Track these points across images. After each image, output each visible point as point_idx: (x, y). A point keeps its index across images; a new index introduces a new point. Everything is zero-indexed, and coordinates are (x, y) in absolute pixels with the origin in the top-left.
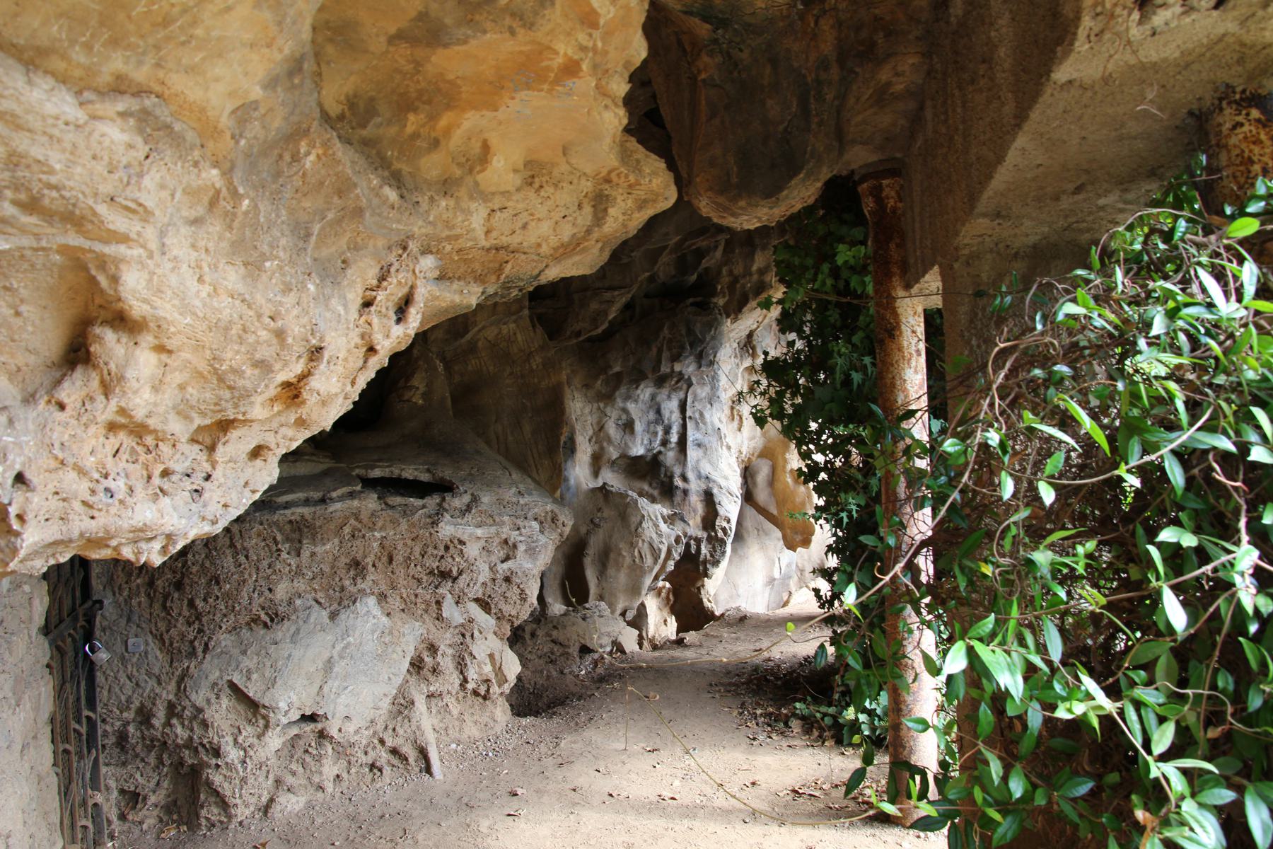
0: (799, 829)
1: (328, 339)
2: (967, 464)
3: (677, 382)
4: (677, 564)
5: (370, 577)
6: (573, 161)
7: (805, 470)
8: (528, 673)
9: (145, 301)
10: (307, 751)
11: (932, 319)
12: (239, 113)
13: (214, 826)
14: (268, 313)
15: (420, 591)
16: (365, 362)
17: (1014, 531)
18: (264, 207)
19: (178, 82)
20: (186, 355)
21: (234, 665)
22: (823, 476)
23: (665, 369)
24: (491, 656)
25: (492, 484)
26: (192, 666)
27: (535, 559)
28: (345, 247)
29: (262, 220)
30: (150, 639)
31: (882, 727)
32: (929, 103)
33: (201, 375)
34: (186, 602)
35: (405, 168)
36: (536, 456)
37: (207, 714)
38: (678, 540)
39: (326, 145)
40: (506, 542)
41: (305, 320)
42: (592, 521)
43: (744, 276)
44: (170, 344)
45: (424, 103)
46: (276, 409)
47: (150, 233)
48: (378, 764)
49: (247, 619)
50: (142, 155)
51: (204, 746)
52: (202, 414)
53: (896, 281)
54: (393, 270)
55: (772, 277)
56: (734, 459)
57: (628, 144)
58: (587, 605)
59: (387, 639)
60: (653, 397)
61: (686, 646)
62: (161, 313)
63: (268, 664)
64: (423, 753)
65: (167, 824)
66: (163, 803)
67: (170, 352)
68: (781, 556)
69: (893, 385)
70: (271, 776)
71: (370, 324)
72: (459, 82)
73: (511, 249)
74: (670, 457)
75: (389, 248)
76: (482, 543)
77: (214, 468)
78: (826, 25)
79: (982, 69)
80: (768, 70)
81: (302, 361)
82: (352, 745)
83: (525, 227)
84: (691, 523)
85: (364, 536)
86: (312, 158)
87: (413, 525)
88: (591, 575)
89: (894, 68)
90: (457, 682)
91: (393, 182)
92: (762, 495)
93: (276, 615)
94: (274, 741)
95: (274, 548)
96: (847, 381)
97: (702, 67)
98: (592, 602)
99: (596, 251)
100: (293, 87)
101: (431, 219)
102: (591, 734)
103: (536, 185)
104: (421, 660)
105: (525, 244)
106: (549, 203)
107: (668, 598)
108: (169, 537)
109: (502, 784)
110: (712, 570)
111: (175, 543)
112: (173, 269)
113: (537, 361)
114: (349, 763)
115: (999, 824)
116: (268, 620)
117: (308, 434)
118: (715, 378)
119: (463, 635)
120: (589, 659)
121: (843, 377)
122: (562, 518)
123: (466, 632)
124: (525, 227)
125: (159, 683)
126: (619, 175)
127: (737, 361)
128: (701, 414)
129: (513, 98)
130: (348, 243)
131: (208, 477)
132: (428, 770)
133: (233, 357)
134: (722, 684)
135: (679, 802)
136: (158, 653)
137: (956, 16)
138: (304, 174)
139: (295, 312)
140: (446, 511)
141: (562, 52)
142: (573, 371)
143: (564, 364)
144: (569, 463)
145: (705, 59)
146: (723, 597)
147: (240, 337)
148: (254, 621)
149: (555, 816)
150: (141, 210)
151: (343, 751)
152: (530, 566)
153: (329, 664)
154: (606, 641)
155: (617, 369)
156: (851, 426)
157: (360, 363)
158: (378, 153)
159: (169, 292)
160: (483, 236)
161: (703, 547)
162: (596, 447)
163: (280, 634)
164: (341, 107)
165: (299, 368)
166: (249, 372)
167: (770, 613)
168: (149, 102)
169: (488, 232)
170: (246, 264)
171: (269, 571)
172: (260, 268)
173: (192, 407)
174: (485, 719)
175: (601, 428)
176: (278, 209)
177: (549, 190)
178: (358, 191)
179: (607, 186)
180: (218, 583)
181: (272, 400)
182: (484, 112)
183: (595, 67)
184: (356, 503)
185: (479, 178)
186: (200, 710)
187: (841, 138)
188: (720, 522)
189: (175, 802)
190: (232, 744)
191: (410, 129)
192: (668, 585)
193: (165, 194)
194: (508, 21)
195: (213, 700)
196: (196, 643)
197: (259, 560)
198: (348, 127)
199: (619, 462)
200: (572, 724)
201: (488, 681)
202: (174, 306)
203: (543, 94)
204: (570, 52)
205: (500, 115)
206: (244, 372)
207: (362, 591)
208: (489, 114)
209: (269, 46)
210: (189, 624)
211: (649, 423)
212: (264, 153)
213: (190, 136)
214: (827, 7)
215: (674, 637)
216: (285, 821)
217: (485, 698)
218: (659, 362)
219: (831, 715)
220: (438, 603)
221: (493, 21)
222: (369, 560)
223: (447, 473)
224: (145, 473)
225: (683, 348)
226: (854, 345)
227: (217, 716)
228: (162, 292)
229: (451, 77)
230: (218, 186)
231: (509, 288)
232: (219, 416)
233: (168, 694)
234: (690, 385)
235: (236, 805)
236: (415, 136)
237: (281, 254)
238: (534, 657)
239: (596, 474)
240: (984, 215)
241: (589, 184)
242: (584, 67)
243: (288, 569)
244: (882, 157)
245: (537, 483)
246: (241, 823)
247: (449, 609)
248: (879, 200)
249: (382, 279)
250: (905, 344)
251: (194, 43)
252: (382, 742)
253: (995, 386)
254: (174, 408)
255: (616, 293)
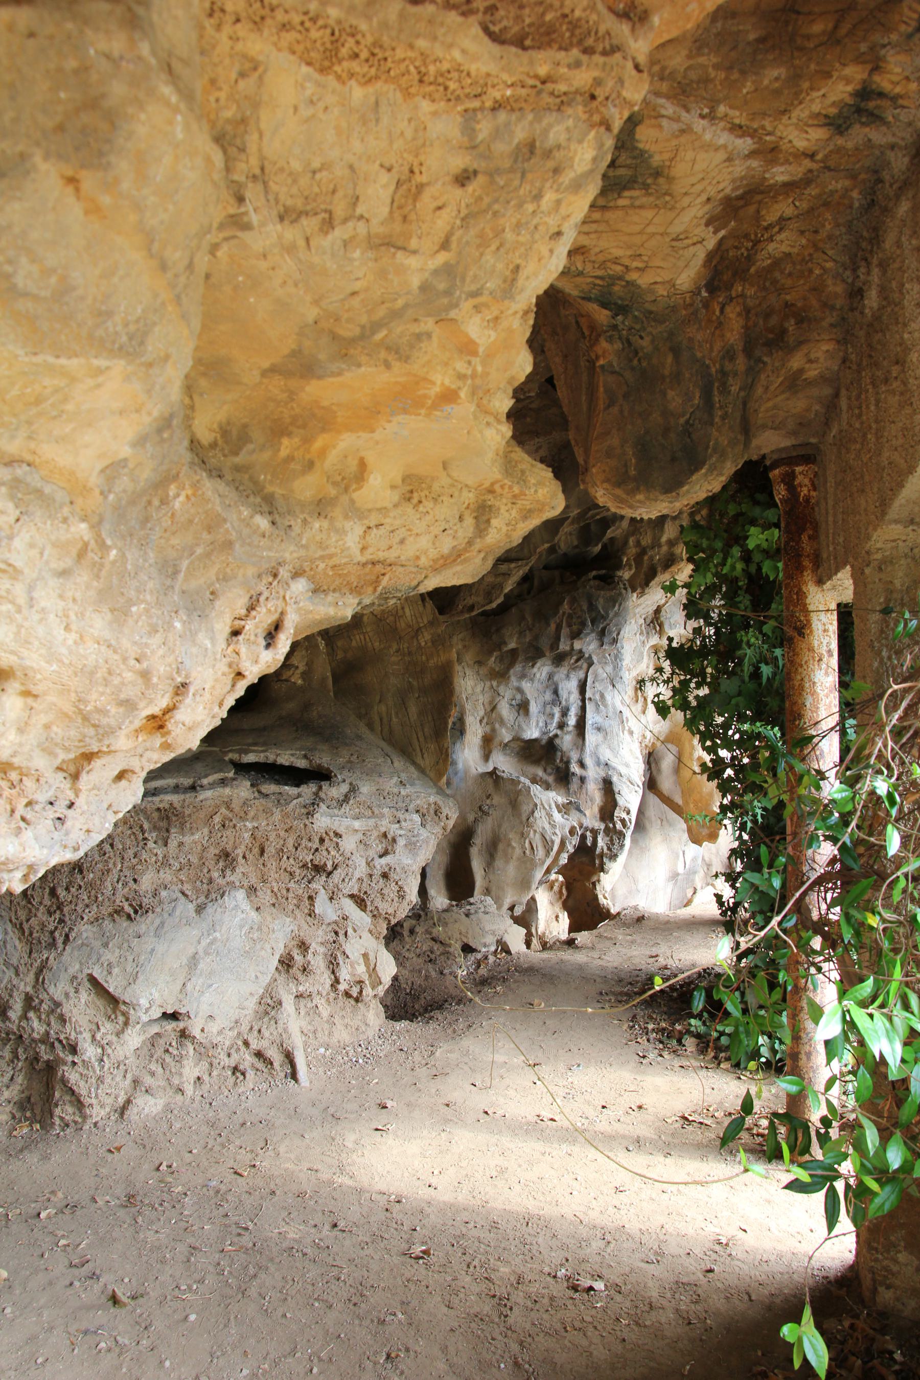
0: (686, 1162)
1: (194, 674)
2: (855, 810)
3: (577, 661)
4: (571, 858)
5: (239, 870)
6: (455, 474)
7: (710, 765)
8: (405, 972)
9: (13, 652)
10: (167, 1051)
11: (845, 614)
12: (108, 472)
13: (67, 1125)
14: (133, 655)
15: (292, 885)
16: (233, 686)
17: (902, 883)
18: (132, 555)
19: (48, 451)
20: (51, 698)
21: (94, 958)
22: (729, 772)
23: (564, 646)
24: (365, 956)
25: (373, 773)
26: (52, 958)
27: (415, 855)
28: (214, 578)
29: (129, 567)
30: (9, 927)
31: (783, 1052)
32: (843, 392)
33: (66, 715)
34: (47, 890)
35: (278, 491)
36: (422, 739)
37: (66, 1009)
38: (572, 831)
39: (195, 486)
40: (385, 835)
41: (171, 659)
42: (480, 808)
43: (653, 548)
44: (35, 690)
45: (298, 427)
46: (140, 739)
47: (19, 590)
48: (241, 1067)
49: (110, 910)
50: (12, 519)
51: (60, 1042)
52: (67, 749)
53: (808, 576)
54: (262, 599)
55: (681, 550)
56: (637, 745)
57: (513, 455)
58: (472, 900)
59: (256, 935)
60: (550, 677)
61: (577, 947)
62: (28, 663)
63: (130, 958)
64: (289, 1058)
65: (20, 1121)
66: (16, 1099)
67: (36, 696)
68: (686, 849)
69: (802, 688)
70: (129, 1076)
71: (237, 653)
72: (334, 408)
73: (388, 561)
74: (567, 741)
75: (259, 576)
76: (360, 836)
77: (77, 796)
78: (732, 312)
79: (895, 370)
80: (670, 359)
81: (168, 695)
82: (214, 1046)
83: (402, 542)
84: (587, 813)
85: (235, 826)
86: (182, 498)
87: (287, 815)
88: (477, 866)
89: (807, 355)
90: (328, 982)
91: (266, 508)
92: (666, 783)
93: (141, 906)
94: (134, 1039)
95: (141, 837)
96: (756, 674)
97: (600, 352)
98: (477, 896)
99: (478, 560)
100: (163, 441)
101: (304, 542)
102: (468, 1042)
103: (415, 501)
104: (291, 958)
105: (402, 558)
106: (428, 518)
107: (560, 892)
108: (31, 868)
109: (372, 1094)
110: (609, 865)
111: (36, 872)
112: (41, 620)
113: (426, 637)
114: (211, 1065)
115: (874, 1194)
116: (132, 912)
117: (172, 755)
118: (618, 657)
119: (336, 933)
120: (472, 957)
121: (752, 669)
122: (445, 811)
123: (339, 931)
124: (402, 542)
125: (17, 974)
126: (502, 487)
127: (643, 638)
128: (602, 696)
129: (390, 421)
130: (217, 574)
131: (71, 805)
132: (294, 1076)
133: (97, 698)
134: (614, 993)
135: (559, 1123)
136: (17, 942)
137: (871, 308)
138: (173, 514)
139: (161, 652)
140: (323, 800)
141: (439, 382)
142: (465, 647)
143: (455, 639)
144: (458, 745)
145: (604, 344)
146: (621, 892)
147: (105, 679)
148: (117, 912)
149: (425, 1132)
150: (10, 569)
151: (205, 1051)
152: (409, 862)
153: (194, 960)
154: (491, 940)
155: (512, 645)
156: (758, 724)
157: (229, 687)
158: (251, 478)
159: (36, 643)
160: (358, 553)
161: (600, 839)
162: (488, 729)
163: (143, 928)
164: (214, 435)
165: (164, 702)
166: (113, 710)
167: (670, 913)
168: (21, 471)
169: (363, 549)
170: (112, 611)
171: (135, 861)
172: (127, 613)
173: (56, 744)
174: (357, 1022)
175: (494, 709)
176: (146, 553)
177: (428, 504)
178: (228, 525)
179: (490, 496)
180: (81, 871)
181: (137, 731)
182: (360, 434)
183: (473, 392)
184: (227, 791)
185: (355, 495)
186: (58, 1004)
187: (746, 429)
188: (619, 814)
189: (29, 1098)
190: (90, 1040)
191: (284, 453)
192: (561, 878)
193: (34, 552)
194: (383, 354)
195: (72, 994)
196: (57, 934)
197: (124, 849)
198: (220, 455)
199: (512, 745)
200: (450, 1031)
201: (360, 982)
202: (40, 655)
203: (420, 418)
204: (447, 382)
205: (377, 435)
206: (108, 711)
207: (231, 884)
208: (365, 435)
209: (137, 411)
210: (50, 914)
211: (545, 705)
212: (132, 502)
213: (60, 496)
214: (734, 294)
215: (564, 936)
216: (141, 1125)
217: (357, 1000)
218: (557, 639)
219: (729, 1035)
220: (311, 898)
221: (368, 355)
222: (240, 851)
223: (323, 759)
224: (8, 807)
225: (583, 624)
226: (764, 635)
227: (75, 1011)
228: (29, 643)
229: (325, 403)
230: (86, 538)
231: (387, 598)
232: (83, 750)
233: (26, 985)
234: (591, 664)
235: (91, 1105)
236: (290, 459)
237: (148, 597)
238: (412, 955)
239: (486, 757)
240: (896, 522)
241: (471, 495)
242: (462, 394)
243: (154, 859)
244: (794, 442)
245: (422, 771)
246: (96, 1124)
247: (322, 905)
248: (792, 489)
249: (251, 608)
250: (816, 643)
251: (65, 416)
252: (246, 1044)
253: (888, 729)
254: (38, 746)
255: (513, 565)
